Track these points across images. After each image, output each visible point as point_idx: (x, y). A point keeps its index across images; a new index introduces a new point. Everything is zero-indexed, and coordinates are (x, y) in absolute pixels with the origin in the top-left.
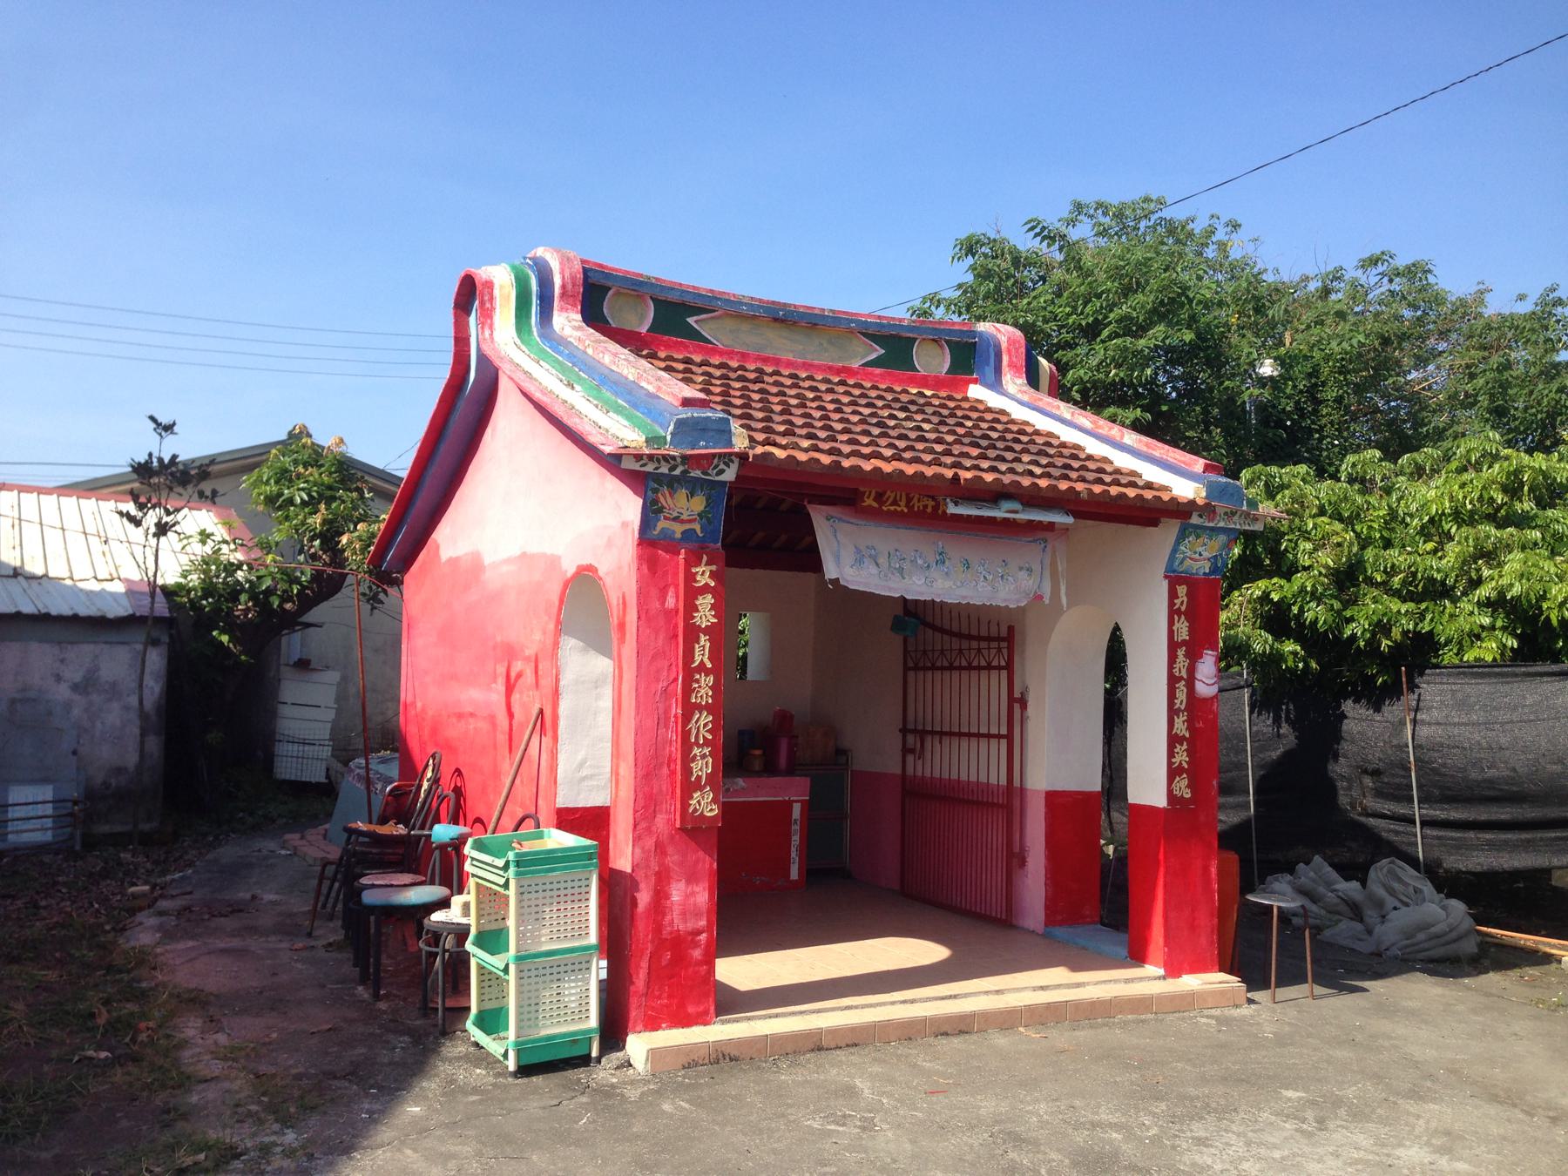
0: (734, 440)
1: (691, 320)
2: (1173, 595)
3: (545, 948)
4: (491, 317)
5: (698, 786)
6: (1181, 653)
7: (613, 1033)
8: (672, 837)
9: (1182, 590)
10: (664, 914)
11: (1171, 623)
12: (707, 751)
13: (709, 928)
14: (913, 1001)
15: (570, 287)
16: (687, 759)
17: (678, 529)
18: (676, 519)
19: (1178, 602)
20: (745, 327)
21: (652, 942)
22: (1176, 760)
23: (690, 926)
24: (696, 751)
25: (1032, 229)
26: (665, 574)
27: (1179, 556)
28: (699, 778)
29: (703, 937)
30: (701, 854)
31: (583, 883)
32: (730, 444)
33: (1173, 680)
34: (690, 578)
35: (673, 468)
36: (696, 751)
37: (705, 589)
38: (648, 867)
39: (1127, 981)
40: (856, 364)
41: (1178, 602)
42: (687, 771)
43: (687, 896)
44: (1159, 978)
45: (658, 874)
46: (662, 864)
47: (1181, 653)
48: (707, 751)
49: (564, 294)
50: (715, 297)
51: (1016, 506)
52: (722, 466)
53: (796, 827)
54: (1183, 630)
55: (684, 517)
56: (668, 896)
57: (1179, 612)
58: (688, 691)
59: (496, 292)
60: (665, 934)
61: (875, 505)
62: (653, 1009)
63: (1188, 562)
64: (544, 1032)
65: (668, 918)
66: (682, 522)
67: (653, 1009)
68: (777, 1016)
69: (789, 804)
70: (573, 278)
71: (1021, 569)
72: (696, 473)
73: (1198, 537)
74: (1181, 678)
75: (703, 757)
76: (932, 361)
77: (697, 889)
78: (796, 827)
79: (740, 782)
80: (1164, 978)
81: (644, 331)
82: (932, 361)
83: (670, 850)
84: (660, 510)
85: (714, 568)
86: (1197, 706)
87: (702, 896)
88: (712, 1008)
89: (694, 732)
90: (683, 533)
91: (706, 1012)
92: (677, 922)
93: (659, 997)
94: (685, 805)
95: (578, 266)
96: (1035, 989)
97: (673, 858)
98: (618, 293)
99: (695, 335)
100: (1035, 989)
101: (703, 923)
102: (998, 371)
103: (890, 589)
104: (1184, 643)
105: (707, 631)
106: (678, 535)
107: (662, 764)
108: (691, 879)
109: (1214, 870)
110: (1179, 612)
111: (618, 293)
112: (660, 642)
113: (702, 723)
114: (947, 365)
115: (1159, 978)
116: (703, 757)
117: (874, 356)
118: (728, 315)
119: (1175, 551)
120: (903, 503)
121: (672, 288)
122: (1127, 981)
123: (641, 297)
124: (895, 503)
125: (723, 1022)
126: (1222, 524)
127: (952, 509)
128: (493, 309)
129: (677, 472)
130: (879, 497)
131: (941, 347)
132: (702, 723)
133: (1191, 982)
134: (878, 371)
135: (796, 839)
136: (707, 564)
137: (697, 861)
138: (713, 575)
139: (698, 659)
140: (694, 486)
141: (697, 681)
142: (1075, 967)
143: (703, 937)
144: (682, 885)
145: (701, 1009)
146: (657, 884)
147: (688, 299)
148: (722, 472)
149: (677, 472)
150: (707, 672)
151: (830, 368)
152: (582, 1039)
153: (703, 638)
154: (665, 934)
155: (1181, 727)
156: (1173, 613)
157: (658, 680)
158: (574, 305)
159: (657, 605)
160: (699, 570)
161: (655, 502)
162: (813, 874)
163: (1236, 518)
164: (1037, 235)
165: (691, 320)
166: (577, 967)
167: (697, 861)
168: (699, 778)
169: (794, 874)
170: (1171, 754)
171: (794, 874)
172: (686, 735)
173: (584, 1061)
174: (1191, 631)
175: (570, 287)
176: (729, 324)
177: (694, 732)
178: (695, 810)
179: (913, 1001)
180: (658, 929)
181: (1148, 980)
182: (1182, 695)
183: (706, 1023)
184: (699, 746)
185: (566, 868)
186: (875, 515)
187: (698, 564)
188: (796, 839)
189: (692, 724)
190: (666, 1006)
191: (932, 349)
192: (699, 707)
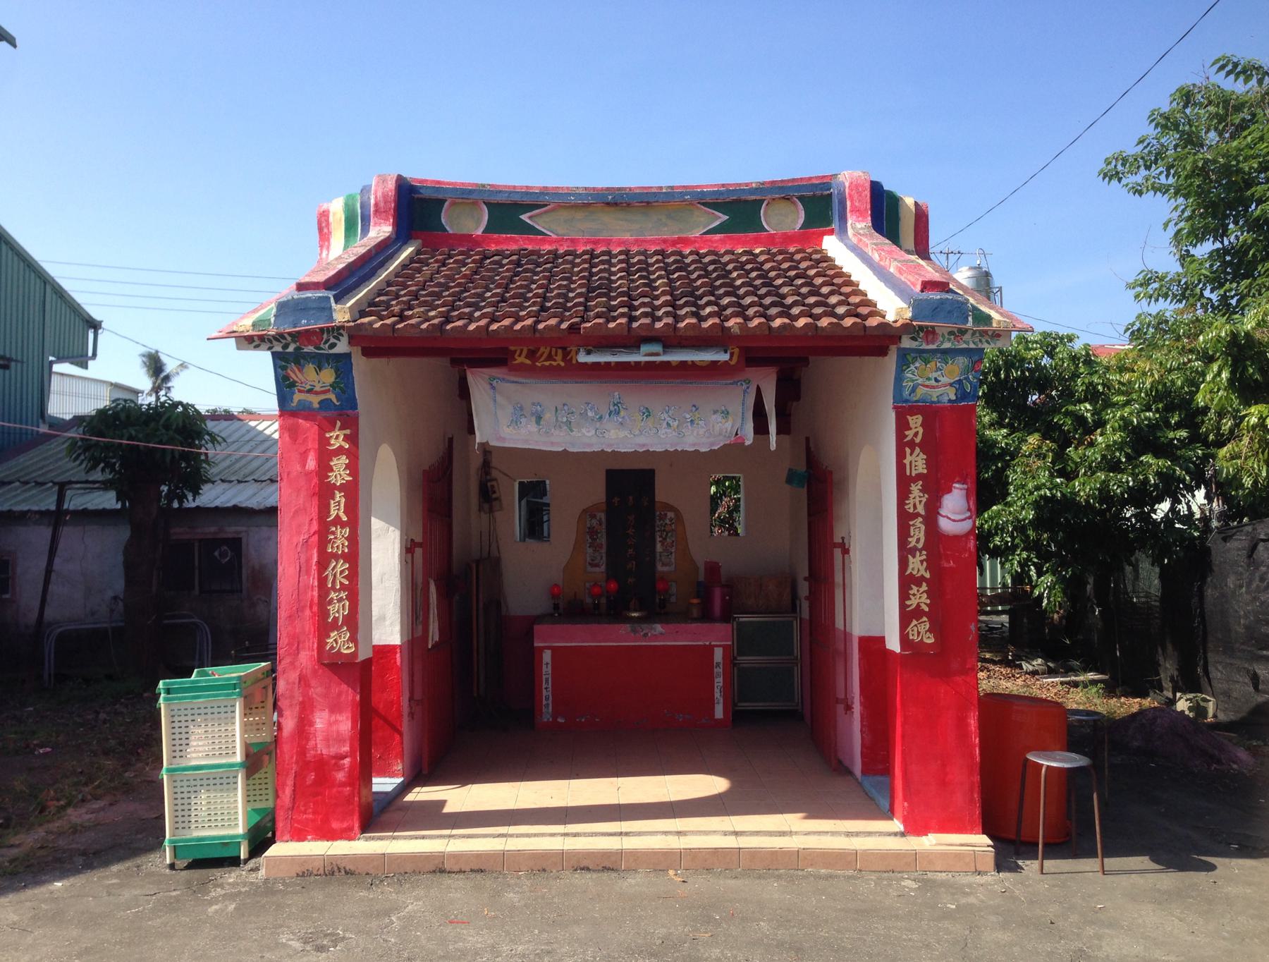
0: (335, 316)
1: (524, 217)
2: (902, 426)
3: (194, 763)
4: (328, 240)
5: (335, 626)
6: (916, 489)
7: (260, 840)
8: (315, 672)
9: (916, 422)
10: (308, 739)
11: (900, 456)
12: (343, 595)
13: (351, 754)
14: (576, 835)
15: (382, 205)
16: (323, 602)
17: (315, 400)
18: (310, 391)
19: (910, 434)
20: (579, 215)
21: (297, 762)
22: (913, 603)
23: (333, 750)
24: (333, 595)
25: (1222, 68)
26: (305, 440)
27: (908, 385)
28: (336, 619)
29: (347, 761)
30: (344, 687)
31: (229, 709)
32: (331, 319)
33: (904, 519)
34: (324, 442)
35: (286, 346)
36: (333, 595)
37: (340, 451)
38: (292, 697)
39: (849, 834)
40: (697, 233)
41: (910, 434)
42: (325, 614)
43: (330, 724)
44: (895, 834)
45: (302, 704)
46: (305, 695)
47: (916, 489)
48: (343, 595)
49: (376, 211)
50: (545, 191)
51: (657, 348)
52: (332, 340)
53: (719, 670)
54: (918, 463)
55: (317, 389)
56: (311, 724)
57: (912, 445)
58: (323, 542)
59: (331, 219)
60: (310, 755)
61: (528, 362)
62: (298, 822)
63: (921, 391)
64: (196, 834)
65: (312, 743)
66: (317, 393)
67: (298, 822)
68: (423, 837)
69: (709, 650)
70: (385, 196)
71: (715, 412)
72: (310, 349)
73: (926, 362)
74: (917, 515)
75: (340, 600)
76: (785, 220)
77: (340, 718)
78: (719, 670)
79: (659, 628)
80: (903, 834)
81: (480, 232)
82: (785, 220)
83: (313, 683)
84: (293, 384)
85: (348, 432)
86: (937, 541)
87: (345, 725)
88: (357, 825)
89: (330, 578)
90: (320, 403)
91: (350, 829)
92: (319, 746)
93: (305, 813)
94: (321, 644)
95: (391, 185)
96: (725, 834)
97: (316, 690)
98: (453, 204)
99: (530, 230)
100: (725, 834)
101: (346, 748)
102: (843, 219)
103: (552, 444)
104: (919, 477)
105: (342, 488)
106: (316, 406)
107: (303, 608)
108: (335, 708)
109: (973, 723)
110: (912, 445)
111: (453, 204)
112: (301, 501)
113: (338, 570)
114: (801, 221)
115: (895, 834)
116: (340, 600)
117: (717, 223)
118: (560, 206)
119: (899, 379)
120: (559, 357)
121: (496, 190)
122: (849, 834)
123: (475, 203)
124: (550, 358)
125: (367, 839)
126: (947, 345)
127: (583, 358)
128: (330, 233)
129: (291, 349)
130: (532, 355)
131: (794, 203)
132: (338, 570)
133: (931, 842)
134: (718, 236)
135: (719, 682)
136: (341, 429)
137: (340, 694)
138: (346, 438)
139: (333, 513)
140: (320, 361)
141: (333, 533)
142: (812, 815)
143: (347, 761)
144: (325, 714)
145: (345, 825)
146: (301, 713)
147: (516, 198)
148: (333, 346)
149: (291, 349)
150: (343, 525)
151: (665, 241)
152: (231, 843)
153: (338, 495)
154: (310, 755)
155: (917, 565)
156: (903, 446)
157: (299, 533)
158: (386, 219)
159: (298, 468)
160: (333, 434)
161: (286, 378)
162: (738, 717)
163: (967, 337)
164: (1228, 73)
165: (524, 217)
166: (225, 781)
167: (340, 694)
168: (336, 619)
169: (719, 712)
170: (904, 595)
171: (719, 712)
172: (322, 581)
173: (234, 862)
174: (928, 463)
175: (382, 205)
176: (564, 215)
177: (330, 578)
178: (332, 648)
179: (576, 835)
180: (302, 752)
181: (878, 836)
182: (918, 533)
183: (350, 839)
184: (335, 590)
185: (209, 696)
186: (530, 371)
187: (333, 429)
188: (719, 682)
189: (329, 571)
190: (313, 821)
191: (783, 207)
192: (335, 556)
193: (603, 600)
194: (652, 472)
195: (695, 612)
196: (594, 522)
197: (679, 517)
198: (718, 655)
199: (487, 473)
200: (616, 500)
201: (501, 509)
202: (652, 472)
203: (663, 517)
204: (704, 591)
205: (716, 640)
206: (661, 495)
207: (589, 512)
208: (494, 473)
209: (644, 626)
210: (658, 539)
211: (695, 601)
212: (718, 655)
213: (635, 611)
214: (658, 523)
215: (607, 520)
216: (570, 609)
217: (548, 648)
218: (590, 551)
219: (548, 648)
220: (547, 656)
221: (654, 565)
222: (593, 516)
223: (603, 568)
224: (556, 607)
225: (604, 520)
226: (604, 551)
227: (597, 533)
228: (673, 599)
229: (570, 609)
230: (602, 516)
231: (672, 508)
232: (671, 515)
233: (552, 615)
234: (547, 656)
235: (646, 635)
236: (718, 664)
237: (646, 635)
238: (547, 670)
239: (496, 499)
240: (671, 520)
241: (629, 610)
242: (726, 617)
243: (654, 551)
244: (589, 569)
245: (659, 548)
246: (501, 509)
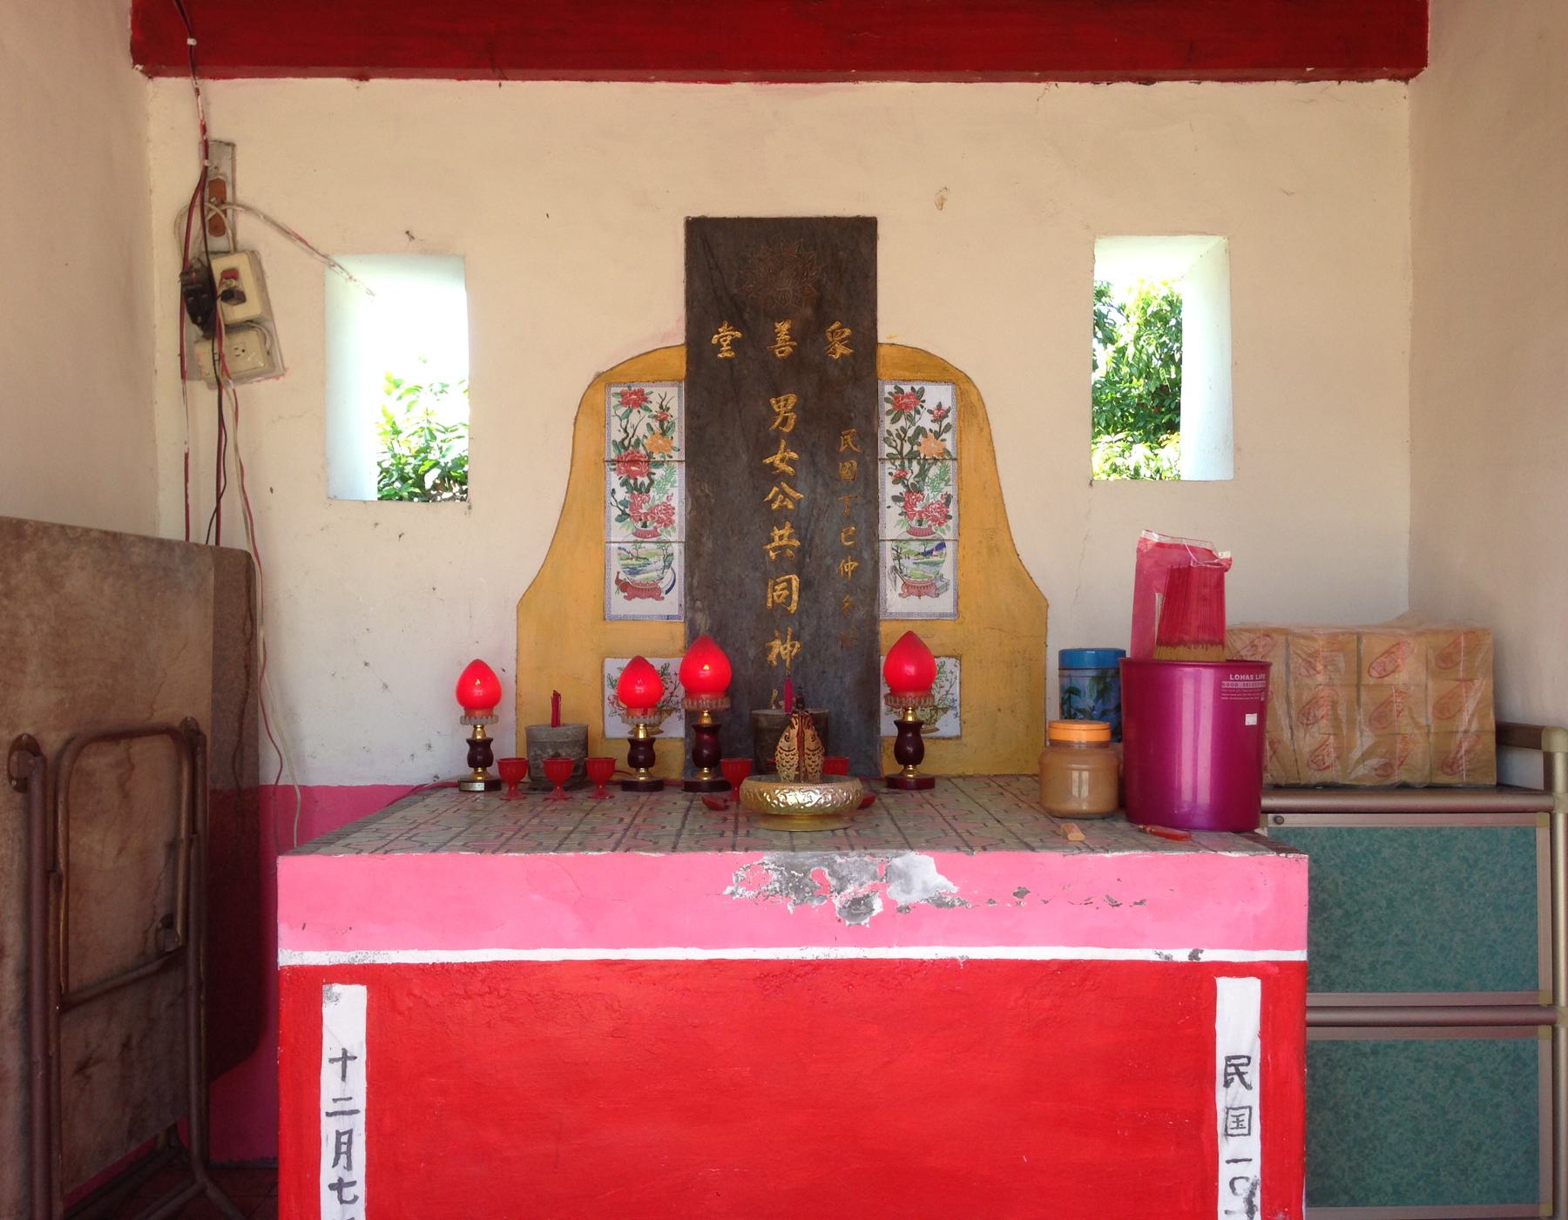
53: (1238, 1100)
69: (1191, 989)
79: (923, 873)
193: (674, 729)
194: (863, 231)
195: (1084, 786)
196: (641, 422)
197: (970, 404)
198: (1238, 1016)
199: (216, 227)
200: (725, 336)
201: (272, 367)
202: (863, 231)
203: (906, 405)
204: (1128, 693)
205: (1219, 922)
206: (901, 317)
207: (622, 384)
208: (246, 228)
209: (846, 861)
210: (889, 489)
211: (1082, 733)
212: (1238, 1016)
213: (803, 777)
214: (887, 425)
215: (691, 413)
216: (536, 776)
217: (348, 974)
218: (621, 533)
219: (348, 974)
220: (345, 1019)
221: (872, 593)
222: (636, 400)
223: (673, 603)
224: (480, 753)
225: (676, 409)
226: (675, 536)
227: (650, 462)
228: (947, 725)
229: (536, 776)
230: (672, 398)
231: (942, 372)
232: (938, 395)
233: (461, 785)
234: (345, 1019)
235: (858, 905)
236: (1236, 1066)
237: (858, 905)
238: (343, 1090)
239: (249, 324)
240: (940, 414)
241: (766, 768)
242: (1237, 815)
243: (872, 536)
244: (620, 604)
245: (892, 524)
246: (272, 367)
